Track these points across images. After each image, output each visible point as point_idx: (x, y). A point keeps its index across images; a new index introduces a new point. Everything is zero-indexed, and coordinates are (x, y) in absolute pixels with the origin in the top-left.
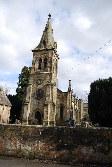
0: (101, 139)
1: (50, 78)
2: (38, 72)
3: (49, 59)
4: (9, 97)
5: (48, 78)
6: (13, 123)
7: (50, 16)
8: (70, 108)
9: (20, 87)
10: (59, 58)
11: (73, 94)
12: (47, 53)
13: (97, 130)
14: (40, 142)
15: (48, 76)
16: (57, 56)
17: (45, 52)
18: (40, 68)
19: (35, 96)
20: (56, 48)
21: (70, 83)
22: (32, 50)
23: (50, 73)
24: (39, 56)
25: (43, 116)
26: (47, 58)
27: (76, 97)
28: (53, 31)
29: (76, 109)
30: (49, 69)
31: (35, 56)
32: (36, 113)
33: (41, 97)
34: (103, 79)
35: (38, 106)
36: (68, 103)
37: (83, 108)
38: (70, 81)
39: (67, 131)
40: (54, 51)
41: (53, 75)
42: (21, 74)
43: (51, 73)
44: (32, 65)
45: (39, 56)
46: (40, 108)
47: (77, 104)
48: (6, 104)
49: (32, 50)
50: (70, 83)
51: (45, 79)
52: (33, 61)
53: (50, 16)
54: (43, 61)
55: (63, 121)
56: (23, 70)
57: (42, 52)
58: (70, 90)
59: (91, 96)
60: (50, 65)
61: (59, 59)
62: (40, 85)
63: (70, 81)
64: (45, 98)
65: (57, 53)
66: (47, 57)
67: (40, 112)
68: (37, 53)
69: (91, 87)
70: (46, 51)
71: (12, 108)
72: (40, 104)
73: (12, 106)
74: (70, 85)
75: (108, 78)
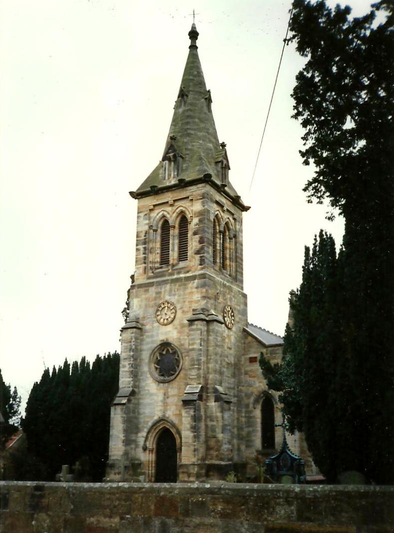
3: (196, 220)
6: (95, 481)
16: (236, 201)
18: (165, 260)
21: (193, 47)
22: (131, 193)
24: (157, 214)
26: (188, 216)
31: (142, 215)
34: (54, 369)
35: (164, 411)
44: (137, 250)
49: (131, 193)
50: (193, 47)
52: (137, 236)
54: (174, 233)
57: (169, 197)
61: (246, 209)
62: (166, 325)
66: (187, 213)
67: (173, 431)
68: (150, 201)
69: (32, 390)
75: (91, 360)
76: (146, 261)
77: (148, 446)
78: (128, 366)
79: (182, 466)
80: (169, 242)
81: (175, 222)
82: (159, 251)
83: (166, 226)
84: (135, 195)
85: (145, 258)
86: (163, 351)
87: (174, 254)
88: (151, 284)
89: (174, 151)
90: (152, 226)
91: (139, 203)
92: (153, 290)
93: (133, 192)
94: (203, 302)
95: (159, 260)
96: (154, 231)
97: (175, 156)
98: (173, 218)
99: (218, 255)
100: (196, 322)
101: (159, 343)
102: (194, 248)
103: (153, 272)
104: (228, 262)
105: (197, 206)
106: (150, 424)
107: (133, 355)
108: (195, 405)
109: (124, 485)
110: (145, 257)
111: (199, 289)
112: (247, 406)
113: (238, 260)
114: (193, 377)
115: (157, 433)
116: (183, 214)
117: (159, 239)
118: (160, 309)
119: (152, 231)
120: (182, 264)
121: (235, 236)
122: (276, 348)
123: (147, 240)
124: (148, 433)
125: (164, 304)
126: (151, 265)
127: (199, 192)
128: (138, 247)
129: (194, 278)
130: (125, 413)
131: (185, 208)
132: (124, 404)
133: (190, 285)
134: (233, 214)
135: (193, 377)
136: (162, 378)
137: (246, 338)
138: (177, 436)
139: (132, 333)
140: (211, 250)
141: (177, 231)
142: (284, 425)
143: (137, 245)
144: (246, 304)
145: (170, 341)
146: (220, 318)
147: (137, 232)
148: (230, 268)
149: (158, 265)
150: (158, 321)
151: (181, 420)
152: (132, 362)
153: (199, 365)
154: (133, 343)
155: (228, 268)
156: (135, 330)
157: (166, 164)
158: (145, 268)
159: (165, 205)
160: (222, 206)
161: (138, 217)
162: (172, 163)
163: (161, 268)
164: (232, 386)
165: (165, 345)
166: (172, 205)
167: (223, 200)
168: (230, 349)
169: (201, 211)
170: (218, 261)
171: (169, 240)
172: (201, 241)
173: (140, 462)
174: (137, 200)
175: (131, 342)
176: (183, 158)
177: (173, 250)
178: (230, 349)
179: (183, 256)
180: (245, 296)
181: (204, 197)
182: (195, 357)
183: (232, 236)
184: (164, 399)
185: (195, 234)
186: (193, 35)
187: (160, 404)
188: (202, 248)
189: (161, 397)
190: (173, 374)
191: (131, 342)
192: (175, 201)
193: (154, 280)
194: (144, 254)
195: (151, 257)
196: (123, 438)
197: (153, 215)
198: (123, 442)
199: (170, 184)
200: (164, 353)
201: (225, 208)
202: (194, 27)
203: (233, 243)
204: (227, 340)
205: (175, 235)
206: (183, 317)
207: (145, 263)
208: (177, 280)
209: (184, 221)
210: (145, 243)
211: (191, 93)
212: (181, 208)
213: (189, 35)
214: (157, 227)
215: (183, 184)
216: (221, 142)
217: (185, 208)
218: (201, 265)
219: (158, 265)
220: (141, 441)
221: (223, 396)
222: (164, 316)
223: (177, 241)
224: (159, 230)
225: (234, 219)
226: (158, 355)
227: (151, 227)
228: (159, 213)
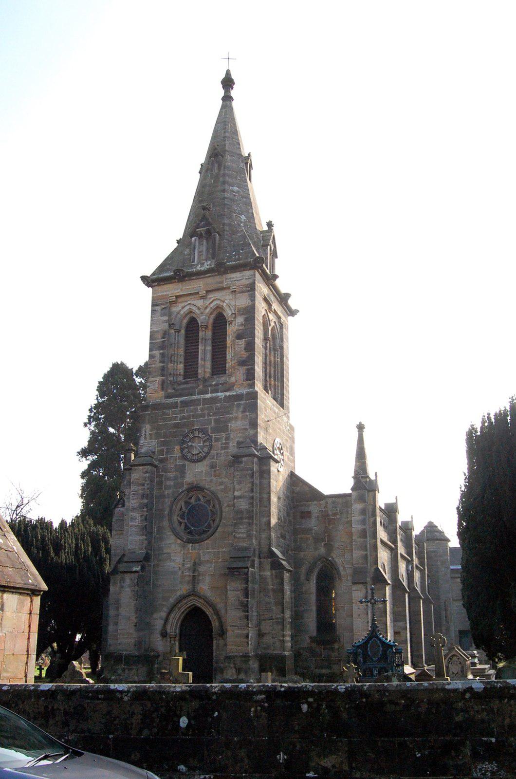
0: (493, 740)
1: (247, 422)
4: (31, 535)
5: (237, 424)
10: (293, 307)
11: (382, 500)
12: (225, 285)
13: (468, 696)
14: (182, 767)
15: (240, 414)
16: (284, 299)
17: (212, 281)
19: (176, 524)
20: (275, 255)
21: (227, 99)
22: (144, 279)
23: (248, 393)
25: (223, 633)
26: (228, 313)
27: (401, 518)
29: (405, 584)
30: (239, 375)
31: (158, 308)
32: (185, 617)
33: (209, 526)
35: (194, 580)
37: (449, 576)
38: (361, 427)
39: (315, 711)
40: (264, 272)
41: (265, 401)
42: (97, 406)
43: (254, 396)
46: (205, 587)
47: (410, 554)
48: (19, 582)
49: (144, 279)
50: (227, 99)
51: (222, 427)
54: (205, 335)
55: (333, 649)
56: (104, 388)
57: (198, 285)
58: (364, 485)
59: (476, 509)
61: (292, 313)
63: (361, 427)
65: (278, 283)
67: (209, 611)
68: (172, 290)
70: (218, 278)
71: (45, 597)
72: (202, 569)
73: (44, 587)
74: (361, 455)
76: (165, 372)
77: (168, 631)
78: (139, 518)
80: (198, 348)
83: (192, 326)
86: (190, 498)
87: (205, 366)
89: (208, 224)
90: (173, 324)
91: (153, 293)
93: (147, 276)
95: (182, 372)
96: (175, 332)
97: (209, 232)
103: (174, 389)
107: (148, 502)
110: (163, 366)
114: (241, 535)
116: (219, 310)
117: (182, 341)
119: (173, 331)
123: (166, 343)
125: (193, 433)
126: (172, 379)
128: (154, 352)
130: (332, 545)
132: (136, 572)
139: (146, 472)
141: (209, 334)
142: (373, 601)
147: (151, 332)
148: (275, 389)
152: (145, 514)
153: (251, 518)
154: (146, 487)
156: (149, 468)
157: (195, 240)
158: (163, 382)
159: (192, 297)
162: (205, 242)
165: (195, 488)
166: (203, 298)
169: (247, 307)
171: (198, 345)
173: (156, 654)
174: (150, 289)
177: (204, 359)
179: (219, 367)
186: (228, 83)
191: (144, 485)
193: (179, 400)
196: (135, 621)
198: (135, 626)
199: (202, 269)
202: (228, 73)
205: (207, 338)
207: (163, 375)
208: (214, 400)
211: (227, 153)
212: (219, 302)
213: (222, 84)
214: (181, 327)
219: (181, 379)
220: (159, 624)
223: (209, 348)
224: (183, 331)
226: (183, 503)
227: (171, 325)
228: (185, 306)
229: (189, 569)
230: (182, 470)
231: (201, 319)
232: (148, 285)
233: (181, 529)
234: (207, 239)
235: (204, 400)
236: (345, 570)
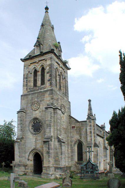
2: (33, 91)
3: (48, 68)
7: (47, 8)
8: (93, 146)
9: (123, 169)
16: (65, 64)
21: (90, 105)
22: (21, 59)
24: (32, 67)
26: (45, 67)
28: (53, 28)
31: (25, 68)
35: (36, 145)
36: (89, 138)
38: (90, 101)
44: (24, 81)
45: (32, 67)
49: (21, 59)
50: (90, 105)
52: (24, 76)
53: (47, 8)
54: (39, 74)
57: (37, 60)
60: (50, 76)
61: (69, 69)
63: (90, 101)
64: (45, 132)
74: (90, 109)
77: (30, 159)
79: (44, 167)
81: (39, 69)
82: (33, 82)
83: (36, 72)
84: (23, 60)
85: (27, 84)
87: (39, 83)
88: (29, 94)
91: (24, 63)
92: (30, 97)
94: (51, 101)
95: (33, 85)
98: (39, 68)
99: (58, 84)
100: (49, 109)
101: (33, 118)
102: (47, 79)
104: (62, 88)
105: (49, 62)
106: (30, 150)
108: (49, 143)
109: (102, 143)
111: (50, 95)
112: (71, 145)
113: (67, 88)
114: (48, 132)
115: (33, 154)
118: (33, 104)
120: (42, 86)
121: (65, 78)
122: (83, 123)
124: (30, 153)
125: (35, 102)
127: (49, 57)
129: (47, 91)
131: (43, 63)
132: (19, 142)
133: (46, 94)
134: (64, 70)
135: (48, 132)
136: (35, 132)
137: (70, 119)
138: (41, 156)
140: (54, 80)
143: (24, 79)
144: (70, 106)
145: (38, 117)
146: (59, 108)
147: (24, 74)
149: (32, 87)
150: (32, 109)
151: (43, 150)
155: (62, 90)
160: (59, 65)
161: (24, 69)
162: (38, 47)
163: (33, 88)
164: (65, 137)
165: (36, 119)
166: (38, 63)
167: (60, 63)
168: (64, 122)
170: (58, 86)
172: (51, 76)
175: (21, 117)
176: (42, 45)
177: (38, 81)
178: (64, 122)
179: (43, 82)
180: (70, 102)
181: (51, 58)
182: (48, 123)
183: (63, 78)
184: (36, 141)
185: (48, 73)
187: (34, 143)
188: (51, 79)
189: (34, 140)
190: (39, 131)
192: (39, 61)
193: (31, 93)
194: (27, 82)
195: (29, 84)
197: (30, 67)
200: (35, 122)
201: (60, 66)
203: (64, 81)
204: (62, 118)
206: (43, 107)
207: (27, 86)
208: (40, 92)
209: (43, 69)
210: (27, 78)
215: (42, 54)
216: (58, 41)
217: (43, 63)
218: (50, 85)
219: (32, 87)
221: (61, 140)
222: (35, 107)
224: (33, 74)
225: (64, 72)
229: (35, 142)
230: (32, 113)
231: (38, 69)
232: (23, 62)
233: (32, 131)
234: (39, 47)
235: (38, 92)
236: (85, 144)
